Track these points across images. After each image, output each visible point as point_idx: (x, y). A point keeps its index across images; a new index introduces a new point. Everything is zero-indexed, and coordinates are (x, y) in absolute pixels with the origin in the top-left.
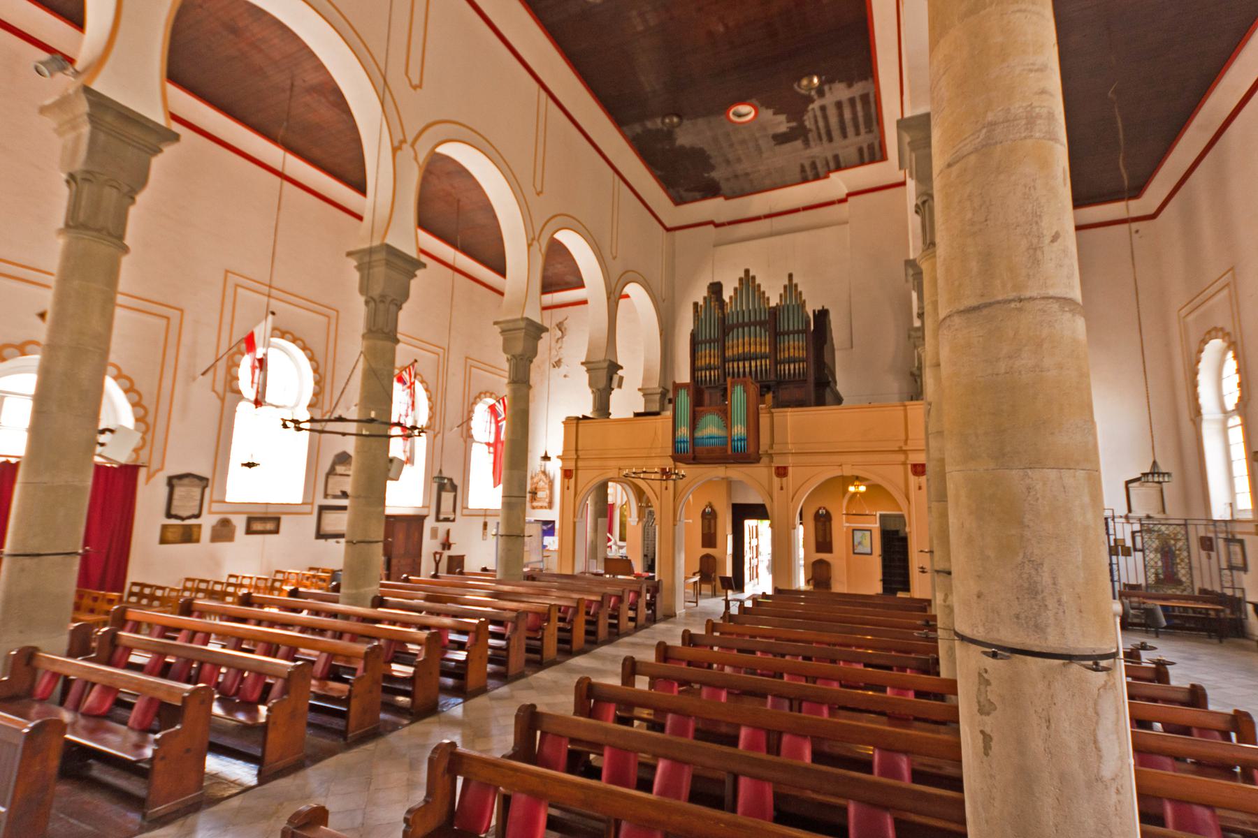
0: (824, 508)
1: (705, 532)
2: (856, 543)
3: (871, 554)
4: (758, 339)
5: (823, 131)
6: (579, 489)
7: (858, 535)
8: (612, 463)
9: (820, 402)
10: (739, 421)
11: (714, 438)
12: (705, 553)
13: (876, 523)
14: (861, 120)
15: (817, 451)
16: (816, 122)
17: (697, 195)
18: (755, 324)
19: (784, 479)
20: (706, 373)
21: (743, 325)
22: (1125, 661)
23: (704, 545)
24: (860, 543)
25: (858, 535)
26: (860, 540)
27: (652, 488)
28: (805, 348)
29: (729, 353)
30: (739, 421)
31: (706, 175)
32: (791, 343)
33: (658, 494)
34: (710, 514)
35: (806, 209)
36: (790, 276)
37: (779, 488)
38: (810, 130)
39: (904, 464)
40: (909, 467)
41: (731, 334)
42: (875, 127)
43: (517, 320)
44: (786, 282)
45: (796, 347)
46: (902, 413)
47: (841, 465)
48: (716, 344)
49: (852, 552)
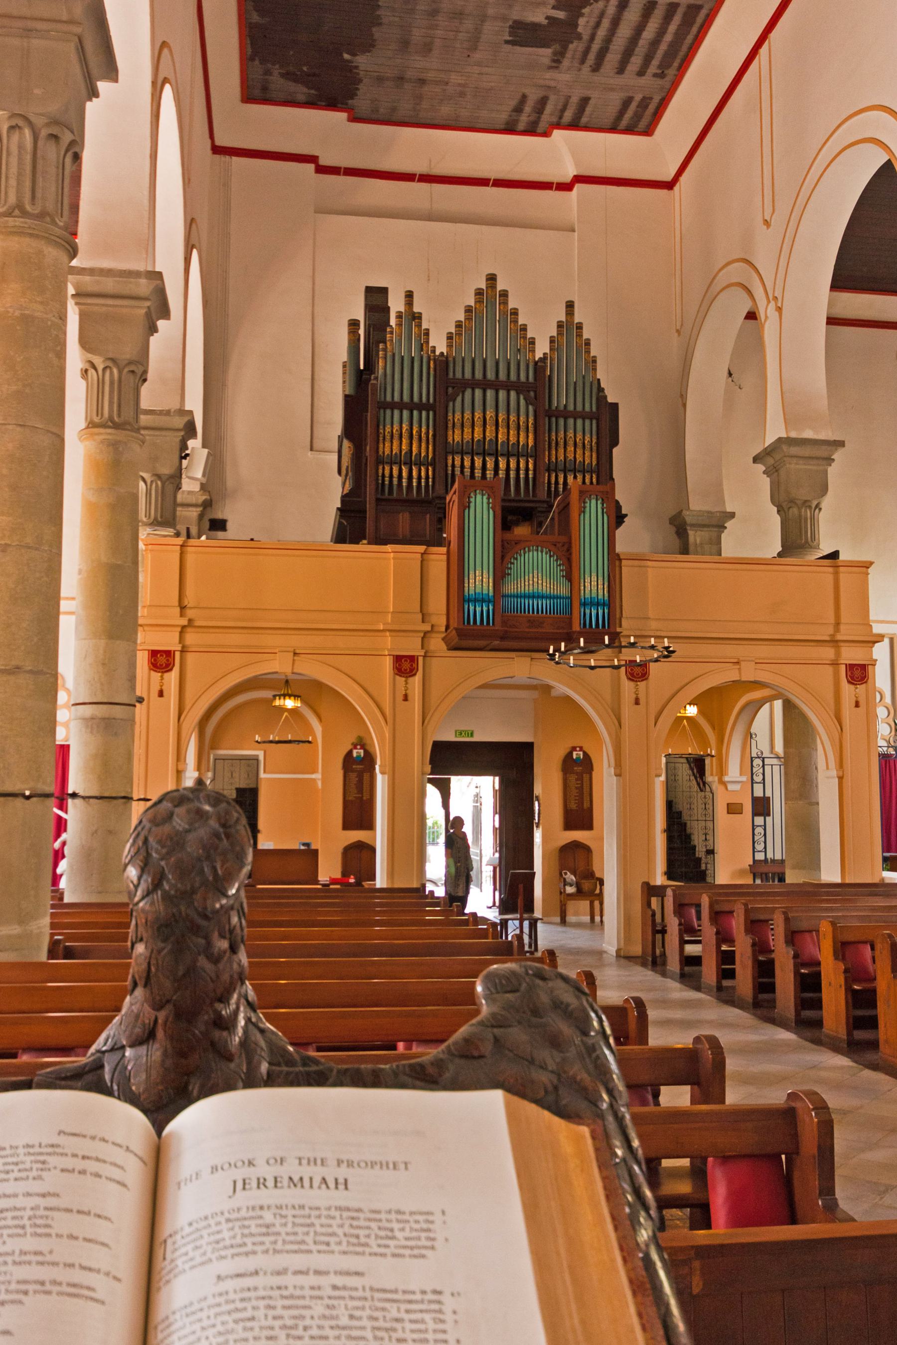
0: (581, 749)
1: (350, 798)
4: (513, 418)
5: (596, 47)
6: (188, 703)
10: (535, 568)
11: (543, 597)
12: (356, 840)
14: (663, 47)
16: (598, 24)
17: (301, 92)
18: (508, 386)
19: (642, 685)
20: (391, 469)
21: (485, 385)
22: (270, 1063)
23: (347, 825)
28: (594, 448)
29: (455, 437)
30: (535, 568)
31: (346, 56)
32: (571, 434)
33: (388, 711)
34: (361, 761)
35: (499, 183)
36: (570, 306)
37: (633, 700)
38: (579, 37)
39: (835, 664)
41: (459, 399)
42: (671, 72)
43: (137, 274)
45: (580, 444)
46: (830, 578)
48: (431, 413)
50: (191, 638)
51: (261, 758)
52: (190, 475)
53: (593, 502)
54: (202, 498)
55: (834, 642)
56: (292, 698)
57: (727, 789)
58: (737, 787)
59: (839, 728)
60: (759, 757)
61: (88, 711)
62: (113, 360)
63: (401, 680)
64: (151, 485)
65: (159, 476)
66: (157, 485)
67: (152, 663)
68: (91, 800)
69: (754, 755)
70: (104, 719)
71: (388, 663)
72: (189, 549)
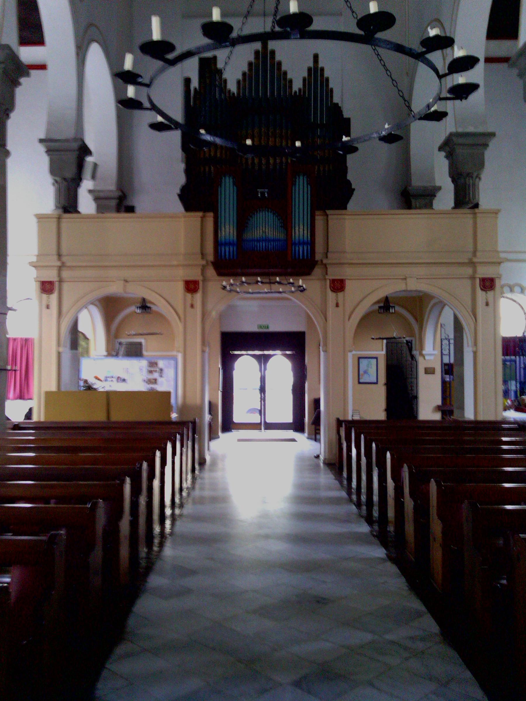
2: (361, 372)
3: (376, 383)
7: (364, 363)
8: (113, 273)
9: (43, 282)
13: (383, 350)
15: (381, 262)
19: (340, 295)
24: (366, 372)
25: (364, 363)
26: (366, 368)
27: (171, 306)
33: (182, 316)
39: (473, 278)
40: (478, 281)
44: (311, 65)
46: (471, 221)
47: (405, 279)
49: (357, 382)
50: (65, 274)
51: (144, 344)
53: (301, 178)
54: (119, 193)
55: (472, 264)
57: (425, 359)
58: (432, 358)
59: (474, 319)
60: (446, 339)
63: (189, 295)
67: (332, 287)
69: (443, 337)
71: (180, 286)
72: (64, 220)
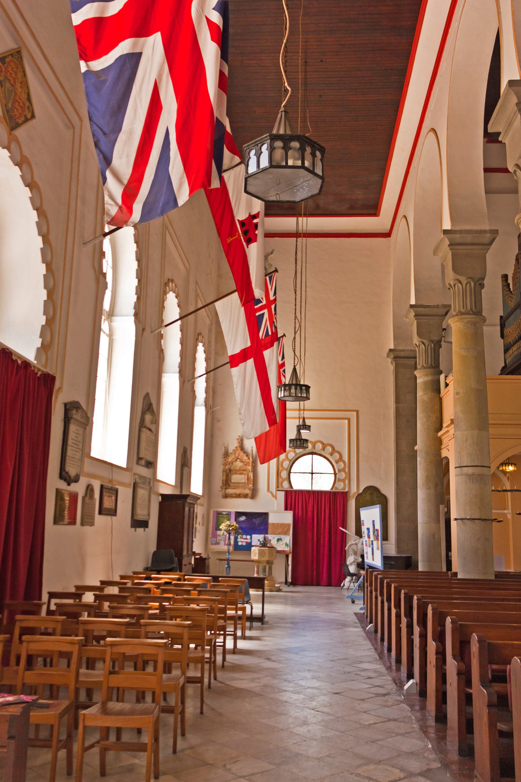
52: (446, 340)
56: (513, 465)
61: (470, 470)
62: (471, 278)
64: (428, 346)
65: (432, 341)
66: (431, 346)
68: (475, 521)
70: (479, 475)
